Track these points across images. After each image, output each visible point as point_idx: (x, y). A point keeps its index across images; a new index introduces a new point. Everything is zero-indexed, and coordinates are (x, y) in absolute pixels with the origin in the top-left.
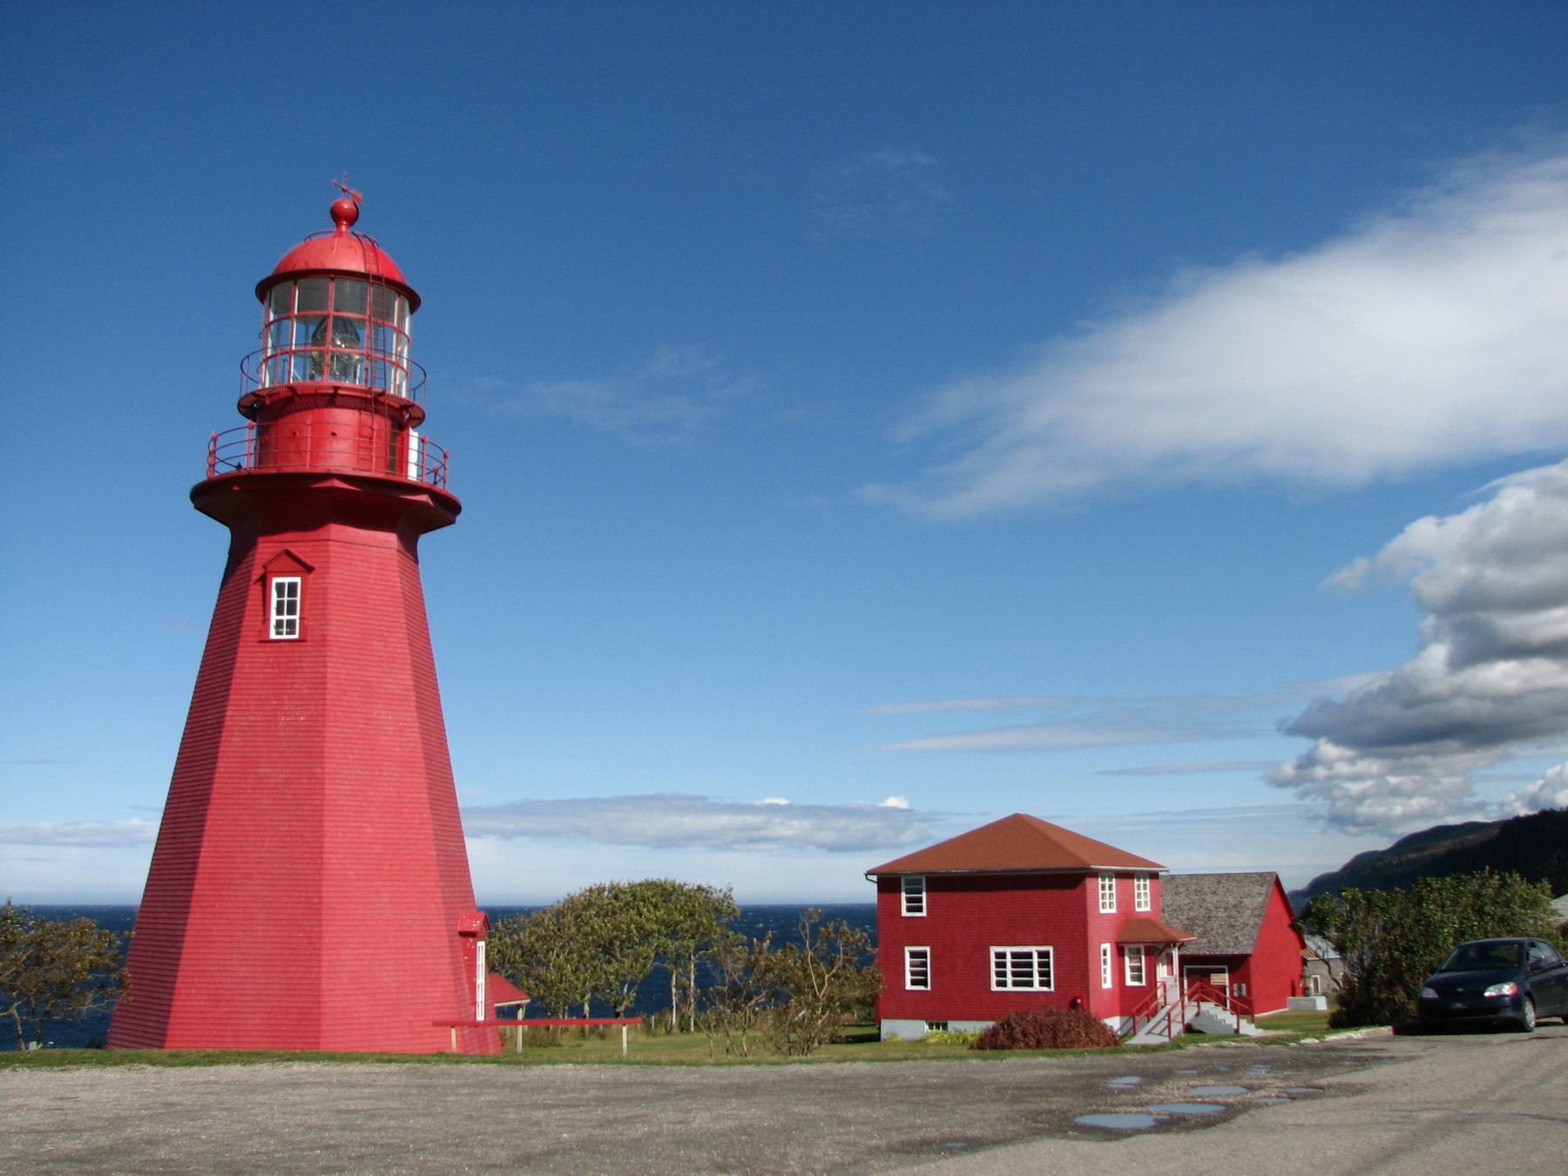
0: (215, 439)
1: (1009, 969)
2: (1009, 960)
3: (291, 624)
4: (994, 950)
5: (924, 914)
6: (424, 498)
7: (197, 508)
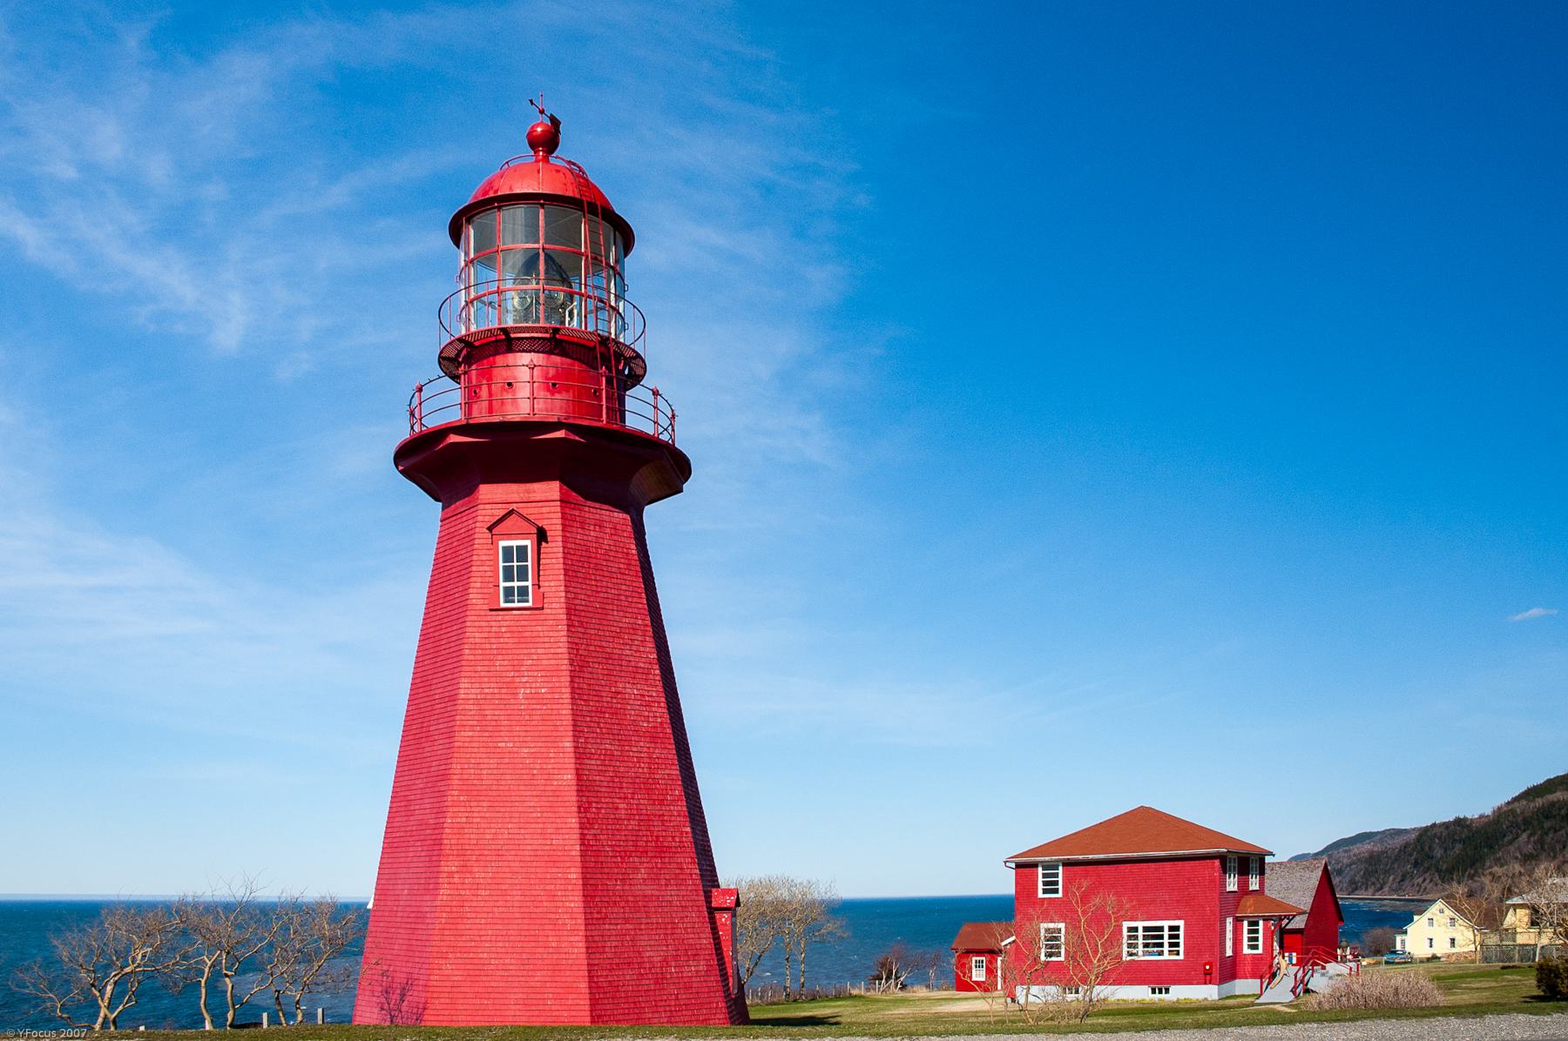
0: (420, 390)
2: (1140, 933)
3: (523, 592)
5: (1060, 895)
6: (560, 434)
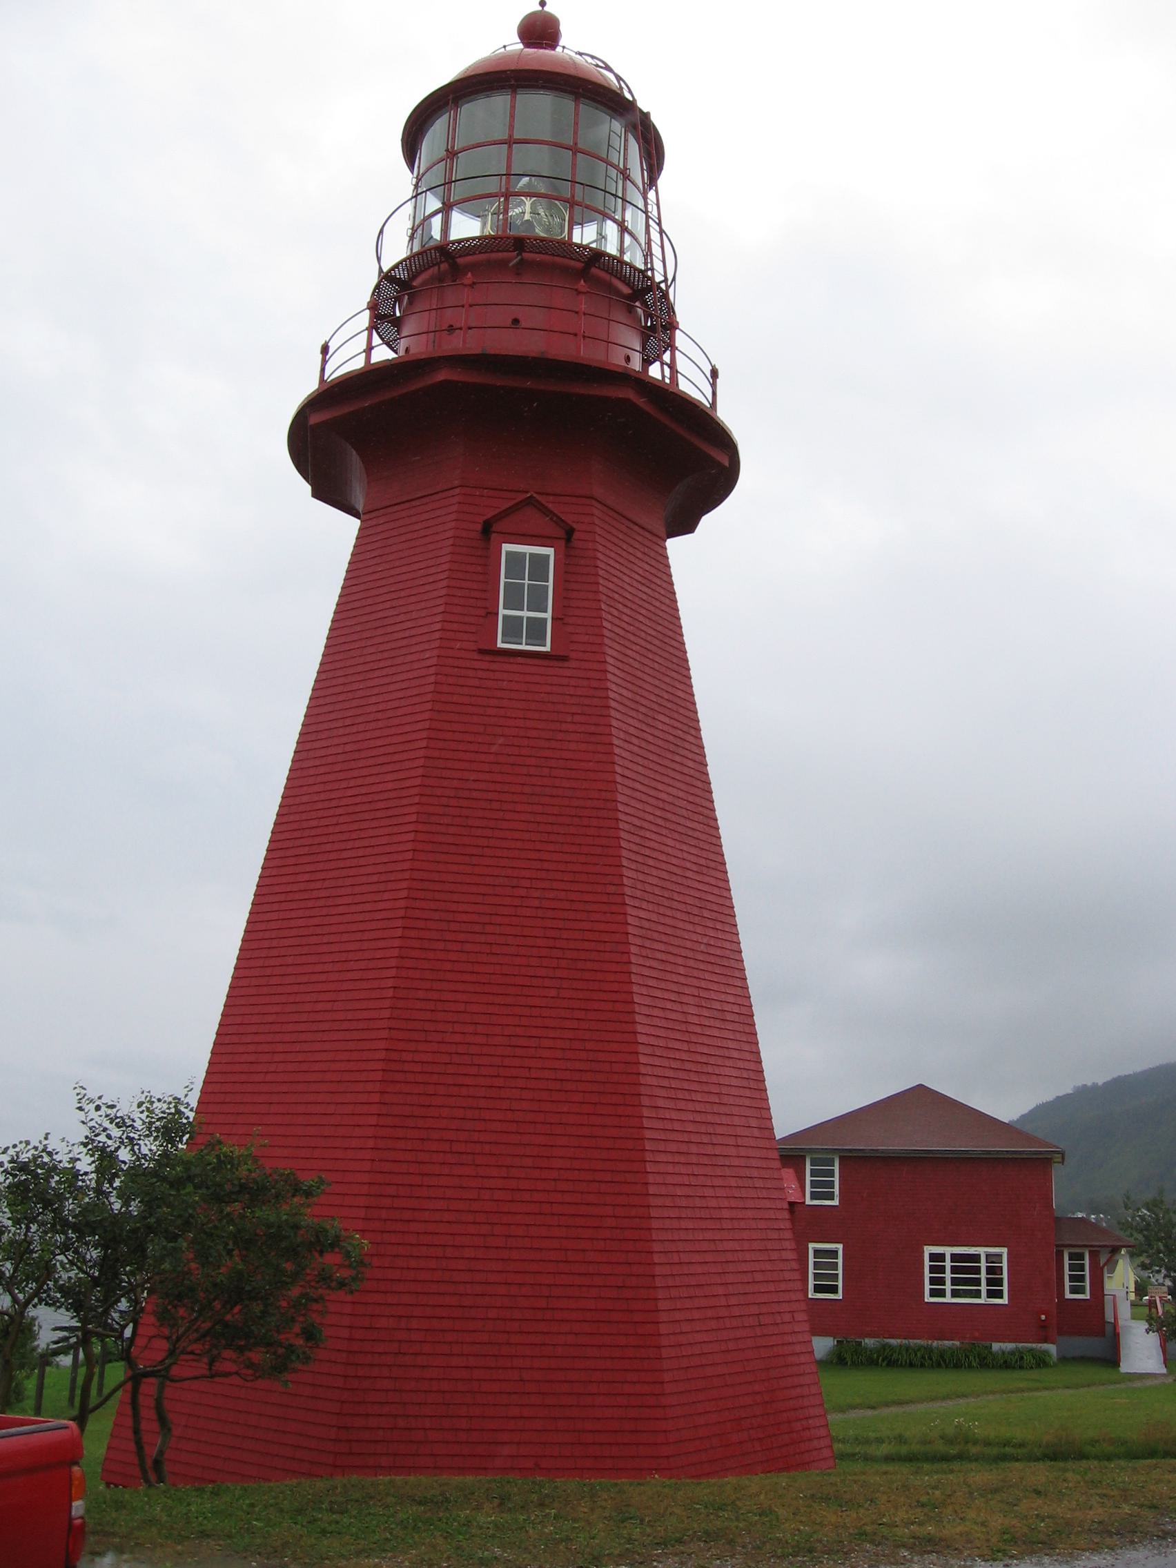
1: (948, 1275)
4: (928, 1250)
7: (317, 494)
